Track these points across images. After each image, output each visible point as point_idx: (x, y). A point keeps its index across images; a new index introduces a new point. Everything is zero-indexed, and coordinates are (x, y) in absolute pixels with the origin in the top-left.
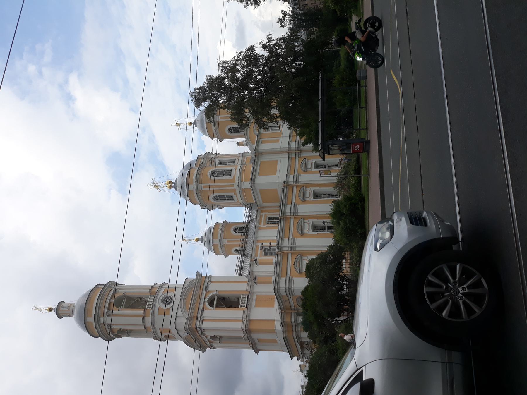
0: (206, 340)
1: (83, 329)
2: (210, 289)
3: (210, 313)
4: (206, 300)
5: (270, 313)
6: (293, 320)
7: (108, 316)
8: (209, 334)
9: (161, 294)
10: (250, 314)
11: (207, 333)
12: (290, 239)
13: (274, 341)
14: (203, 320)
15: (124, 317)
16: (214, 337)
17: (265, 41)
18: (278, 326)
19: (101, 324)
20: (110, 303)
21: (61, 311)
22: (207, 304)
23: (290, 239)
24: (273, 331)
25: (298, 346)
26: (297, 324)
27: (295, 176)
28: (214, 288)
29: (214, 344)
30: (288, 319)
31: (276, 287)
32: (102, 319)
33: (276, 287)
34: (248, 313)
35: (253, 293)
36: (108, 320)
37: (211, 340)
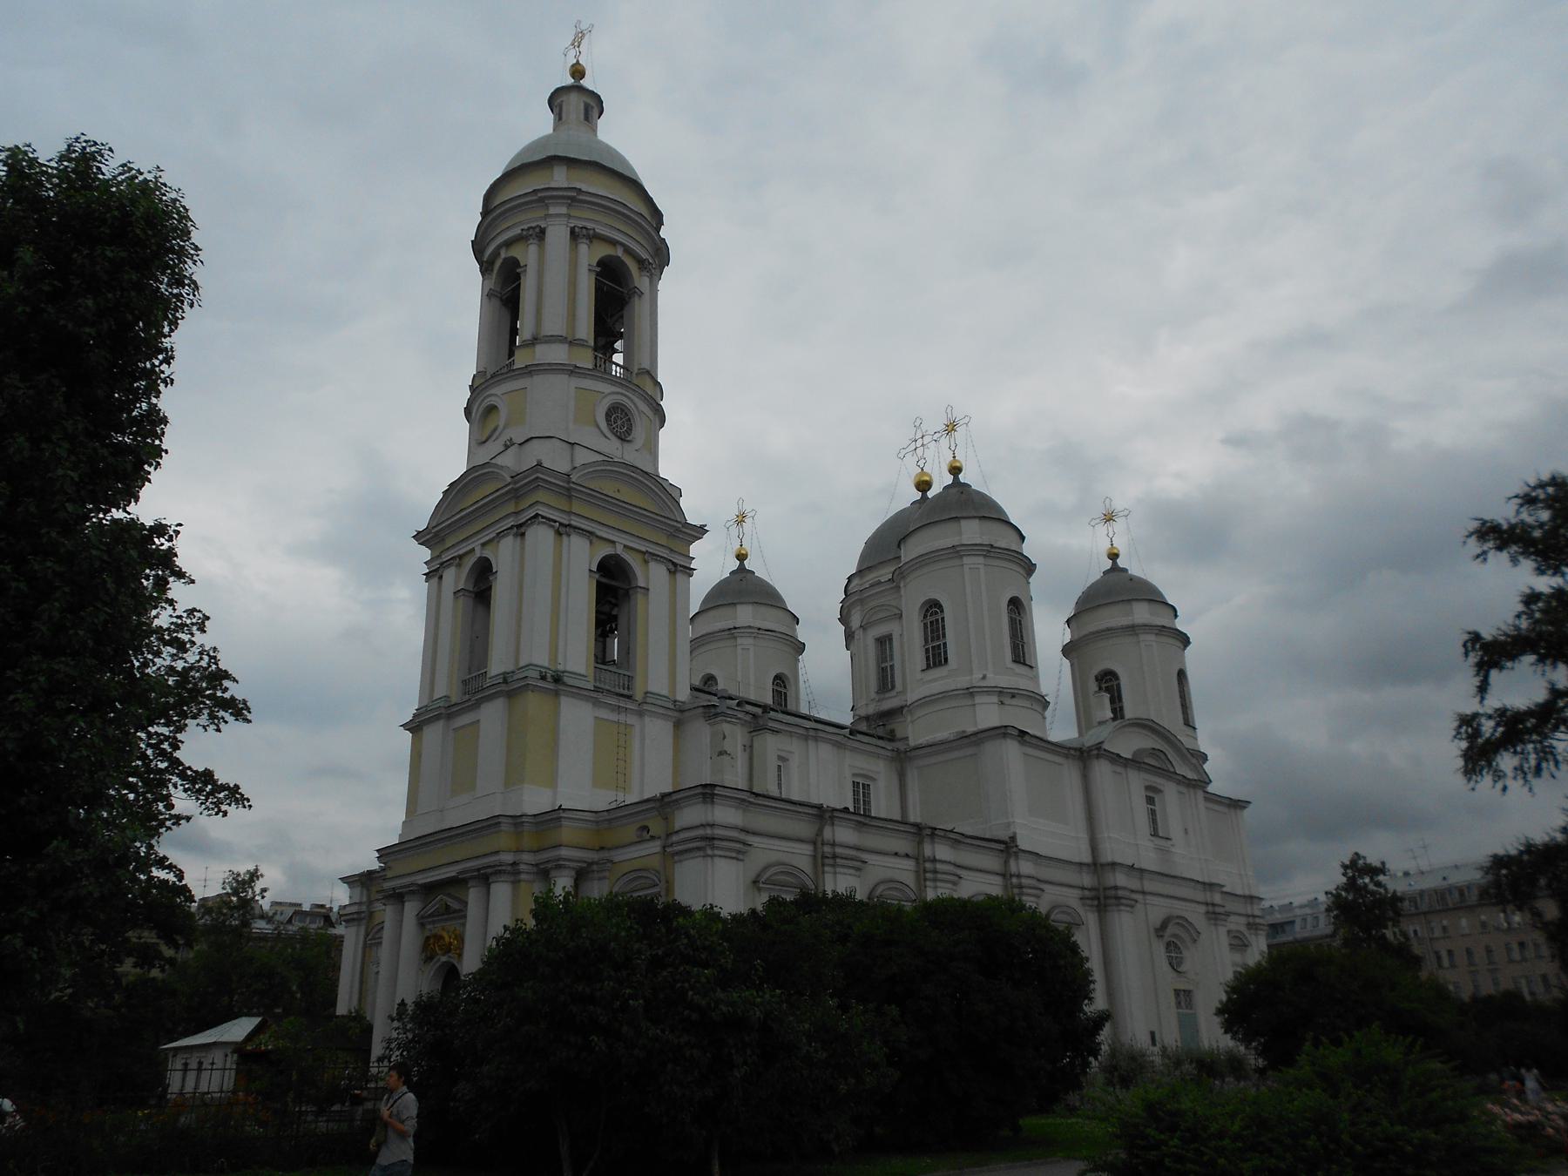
0: (475, 544)
1: (519, 155)
2: (652, 565)
3: (582, 558)
4: (619, 550)
5: (577, 769)
6: (564, 852)
8: (504, 556)
9: (639, 406)
10: (573, 695)
11: (508, 543)
12: (742, 836)
13: (462, 778)
14: (558, 533)
15: (560, 287)
16: (484, 571)
17: (222, 726)
18: (535, 800)
19: (547, 207)
20: (614, 243)
21: (576, 100)
22: (604, 551)
23: (742, 836)
24: (514, 776)
25: (450, 872)
26: (544, 873)
27: (734, 834)
28: (654, 577)
29: (449, 575)
30: (567, 832)
31: (674, 797)
32: (564, 210)
33: (674, 797)
34: (578, 693)
35: (641, 714)
36: (558, 234)
37: (469, 562)
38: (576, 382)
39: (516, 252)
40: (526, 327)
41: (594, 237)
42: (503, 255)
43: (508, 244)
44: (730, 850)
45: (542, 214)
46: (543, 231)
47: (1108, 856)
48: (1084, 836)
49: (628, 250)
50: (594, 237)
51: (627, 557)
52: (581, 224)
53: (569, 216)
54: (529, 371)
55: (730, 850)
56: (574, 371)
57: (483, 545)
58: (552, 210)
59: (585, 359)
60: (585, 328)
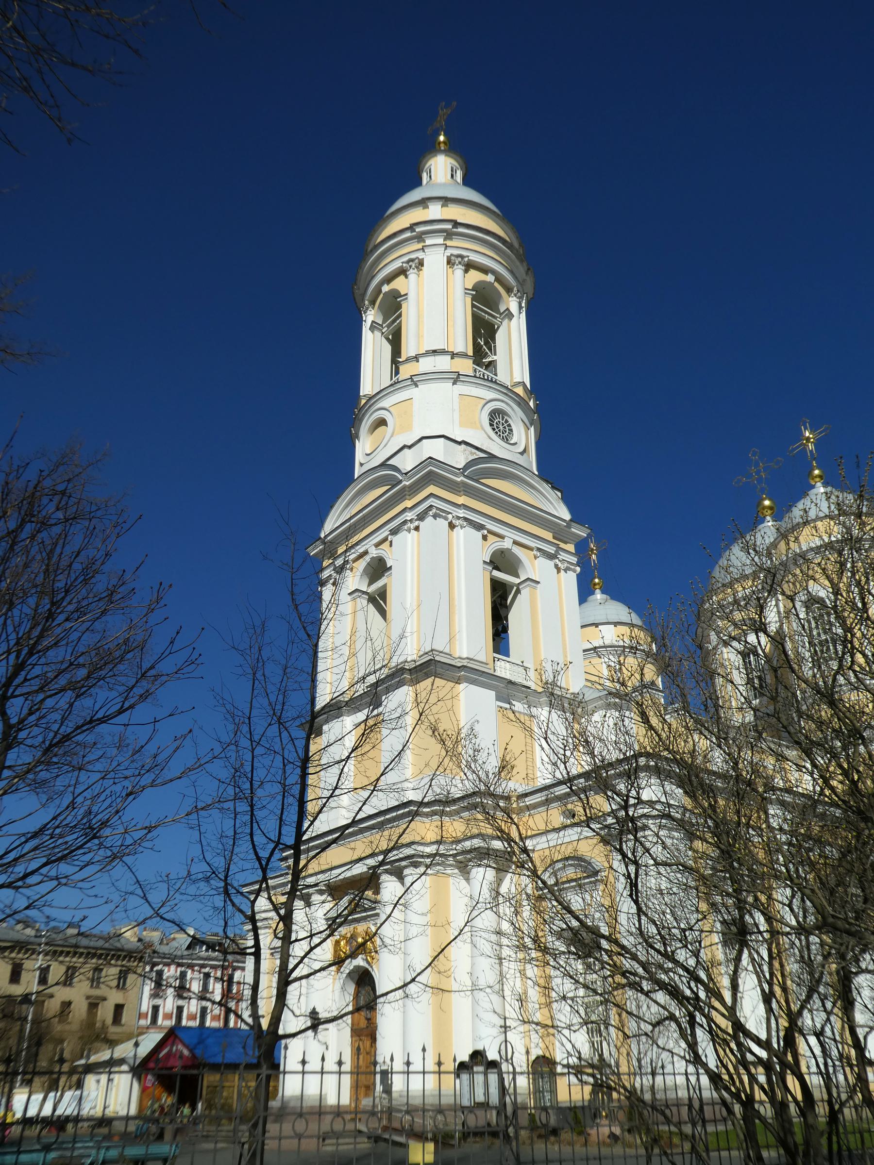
0: (368, 545)
7: (449, 262)
20: (485, 270)
22: (494, 544)
32: (440, 241)
38: (460, 388)
39: (399, 284)
40: (409, 348)
41: (469, 266)
42: (385, 288)
43: (389, 279)
44: (510, 397)
45: (420, 246)
46: (421, 263)
47: (286, 1075)
48: (330, 1070)
49: (499, 279)
50: (469, 266)
51: (517, 550)
52: (456, 252)
53: (446, 247)
54: (414, 381)
55: (510, 397)
56: (457, 378)
57: (377, 545)
58: (429, 242)
59: (466, 366)
60: (462, 341)
